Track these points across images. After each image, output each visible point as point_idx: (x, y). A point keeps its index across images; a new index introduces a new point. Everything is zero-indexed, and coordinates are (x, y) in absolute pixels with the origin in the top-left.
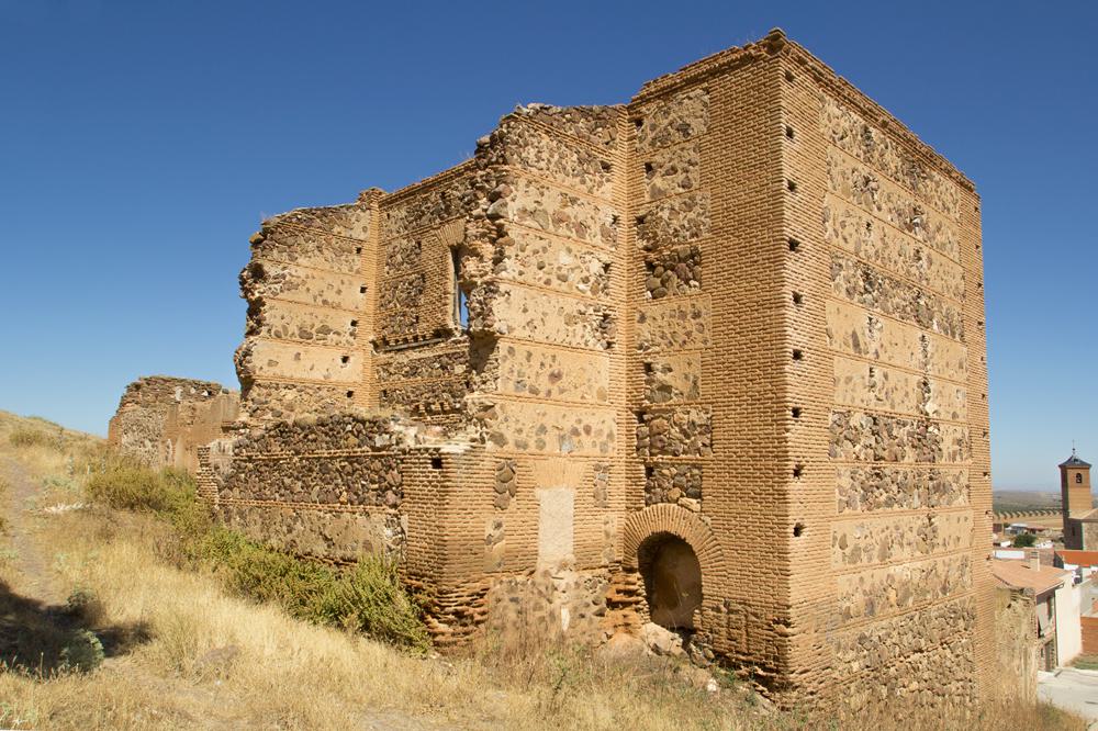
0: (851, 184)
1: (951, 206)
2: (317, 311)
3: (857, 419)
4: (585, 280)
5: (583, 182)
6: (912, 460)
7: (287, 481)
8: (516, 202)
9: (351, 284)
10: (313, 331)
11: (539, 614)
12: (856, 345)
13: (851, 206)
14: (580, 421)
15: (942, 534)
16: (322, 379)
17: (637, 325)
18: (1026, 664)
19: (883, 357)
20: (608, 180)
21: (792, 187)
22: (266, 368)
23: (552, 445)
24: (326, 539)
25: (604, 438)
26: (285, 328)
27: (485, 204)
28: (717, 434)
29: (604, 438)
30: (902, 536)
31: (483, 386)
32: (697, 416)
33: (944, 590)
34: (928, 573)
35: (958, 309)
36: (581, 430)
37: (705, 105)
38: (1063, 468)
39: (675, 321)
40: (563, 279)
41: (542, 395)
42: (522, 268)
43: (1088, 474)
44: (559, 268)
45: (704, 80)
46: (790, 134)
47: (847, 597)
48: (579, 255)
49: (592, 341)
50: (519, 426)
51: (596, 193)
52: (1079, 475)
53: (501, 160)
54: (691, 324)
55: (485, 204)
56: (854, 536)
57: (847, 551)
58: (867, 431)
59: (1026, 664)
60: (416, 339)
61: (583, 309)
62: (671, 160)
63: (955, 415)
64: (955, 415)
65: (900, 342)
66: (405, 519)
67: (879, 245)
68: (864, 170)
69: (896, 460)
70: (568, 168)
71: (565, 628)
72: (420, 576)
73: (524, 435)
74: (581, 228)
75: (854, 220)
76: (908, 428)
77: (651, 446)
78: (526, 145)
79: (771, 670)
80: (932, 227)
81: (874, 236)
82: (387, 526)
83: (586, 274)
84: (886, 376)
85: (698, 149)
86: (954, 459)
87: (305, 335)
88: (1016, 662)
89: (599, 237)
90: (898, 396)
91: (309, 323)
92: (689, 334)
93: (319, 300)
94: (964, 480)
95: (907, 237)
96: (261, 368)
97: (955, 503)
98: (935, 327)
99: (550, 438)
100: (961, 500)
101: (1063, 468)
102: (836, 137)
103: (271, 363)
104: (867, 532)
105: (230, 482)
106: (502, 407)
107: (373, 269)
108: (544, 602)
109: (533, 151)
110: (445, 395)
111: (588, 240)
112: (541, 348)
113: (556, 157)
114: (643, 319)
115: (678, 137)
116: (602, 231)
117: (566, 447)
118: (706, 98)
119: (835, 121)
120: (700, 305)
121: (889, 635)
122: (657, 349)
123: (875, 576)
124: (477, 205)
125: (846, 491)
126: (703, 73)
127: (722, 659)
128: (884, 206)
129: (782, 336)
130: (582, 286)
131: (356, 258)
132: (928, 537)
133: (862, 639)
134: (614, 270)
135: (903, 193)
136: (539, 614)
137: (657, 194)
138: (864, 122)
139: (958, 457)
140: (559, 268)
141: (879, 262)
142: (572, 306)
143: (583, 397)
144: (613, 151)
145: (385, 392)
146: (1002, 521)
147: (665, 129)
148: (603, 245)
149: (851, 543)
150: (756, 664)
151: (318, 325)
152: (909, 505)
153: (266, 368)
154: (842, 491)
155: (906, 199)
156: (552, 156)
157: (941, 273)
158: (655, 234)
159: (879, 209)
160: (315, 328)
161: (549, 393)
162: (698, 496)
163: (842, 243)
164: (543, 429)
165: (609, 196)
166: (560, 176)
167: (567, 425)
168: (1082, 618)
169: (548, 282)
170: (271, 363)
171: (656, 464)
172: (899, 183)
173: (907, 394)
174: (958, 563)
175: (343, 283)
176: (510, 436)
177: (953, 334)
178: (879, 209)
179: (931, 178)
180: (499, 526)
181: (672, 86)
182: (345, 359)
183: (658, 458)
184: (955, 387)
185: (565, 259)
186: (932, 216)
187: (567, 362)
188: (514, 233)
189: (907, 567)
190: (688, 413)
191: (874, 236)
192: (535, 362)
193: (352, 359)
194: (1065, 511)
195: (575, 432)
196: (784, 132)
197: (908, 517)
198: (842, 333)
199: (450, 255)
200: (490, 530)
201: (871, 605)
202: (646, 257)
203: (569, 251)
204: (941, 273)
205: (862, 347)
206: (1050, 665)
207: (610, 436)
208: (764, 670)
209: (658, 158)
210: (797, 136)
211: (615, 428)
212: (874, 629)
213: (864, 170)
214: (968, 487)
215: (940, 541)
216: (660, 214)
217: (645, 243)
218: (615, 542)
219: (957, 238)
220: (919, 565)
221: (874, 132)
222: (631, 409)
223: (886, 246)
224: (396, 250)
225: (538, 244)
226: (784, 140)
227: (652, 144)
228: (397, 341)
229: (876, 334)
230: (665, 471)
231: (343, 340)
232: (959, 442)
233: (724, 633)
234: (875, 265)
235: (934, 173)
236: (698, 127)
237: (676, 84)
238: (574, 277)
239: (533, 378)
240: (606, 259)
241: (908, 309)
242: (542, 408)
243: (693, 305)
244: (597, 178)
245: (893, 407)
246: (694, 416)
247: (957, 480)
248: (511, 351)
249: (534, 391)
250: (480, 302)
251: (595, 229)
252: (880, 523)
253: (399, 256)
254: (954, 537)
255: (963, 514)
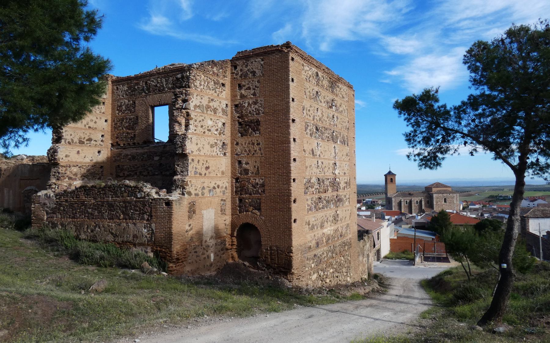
0: (312, 95)
1: (345, 96)
2: (86, 132)
3: (314, 180)
4: (217, 130)
5: (216, 92)
6: (331, 192)
7: (90, 210)
8: (194, 101)
9: (101, 118)
10: (85, 141)
11: (204, 256)
12: (313, 153)
13: (312, 103)
14: (216, 184)
15: (340, 216)
16: (89, 161)
17: (235, 146)
18: (368, 260)
19: (322, 156)
20: (224, 90)
21: (293, 100)
22: (64, 158)
23: (207, 194)
24: (112, 234)
25: (224, 189)
26: (72, 140)
27: (181, 103)
28: (266, 187)
29: (224, 189)
30: (327, 219)
31: (182, 173)
32: (259, 181)
33: (341, 236)
34: (336, 230)
35: (346, 134)
36: (216, 187)
37: (262, 65)
38: (386, 176)
39: (250, 145)
40: (209, 130)
41: (203, 175)
42: (196, 128)
43: (395, 178)
44: (208, 127)
45: (261, 55)
46: (293, 80)
47: (310, 242)
48: (214, 121)
49: (219, 153)
50: (196, 188)
51: (220, 96)
52: (392, 179)
53: (187, 86)
54: (257, 148)
55: (181, 103)
56: (312, 220)
57: (310, 226)
58: (316, 184)
59: (368, 260)
60: (134, 144)
61: (216, 141)
62: (248, 84)
63: (345, 173)
64: (345, 173)
65: (327, 150)
66: (153, 225)
67: (321, 116)
68: (316, 89)
69: (325, 192)
70: (211, 87)
71: (212, 260)
72: (161, 247)
73: (197, 191)
74: (215, 110)
75: (313, 108)
76: (329, 180)
77: (241, 190)
78: (196, 80)
79: (287, 269)
80: (338, 105)
81: (319, 113)
82: (145, 228)
83: (217, 128)
84: (322, 163)
85: (258, 82)
86: (344, 189)
87: (81, 142)
88: (365, 259)
89: (221, 113)
90: (326, 170)
91: (83, 137)
92: (255, 151)
93: (87, 126)
94: (347, 197)
95: (330, 111)
96: (62, 158)
97: (345, 205)
98: (339, 142)
99: (206, 191)
100: (347, 203)
101: (386, 176)
102: (307, 78)
103: (66, 156)
104: (316, 219)
105: (54, 211)
106: (190, 181)
107: (110, 111)
108: (205, 252)
109: (198, 82)
110: (149, 169)
111: (217, 115)
112: (203, 158)
113: (206, 83)
114: (237, 144)
115: (250, 75)
116: (222, 110)
117: (211, 193)
118: (262, 62)
119: (307, 72)
120: (260, 141)
121: (323, 253)
122: (243, 155)
123: (319, 233)
124: (178, 104)
125: (309, 205)
126: (261, 53)
127: (269, 266)
128: (322, 101)
129: (289, 154)
130: (216, 133)
131: (102, 106)
132: (336, 219)
133: (315, 255)
134: (226, 125)
135: (329, 95)
136: (204, 256)
137: (242, 96)
138: (316, 71)
139: (346, 188)
140: (208, 127)
141: (321, 122)
142: (212, 141)
143: (216, 175)
144: (226, 78)
145: (119, 166)
146: (362, 198)
147: (246, 71)
148: (222, 116)
149: (311, 223)
150: (282, 267)
151: (87, 138)
152: (330, 208)
153: (64, 158)
154: (308, 205)
155: (330, 97)
156: (205, 83)
157: (341, 122)
158: (242, 112)
159: (321, 102)
160: (86, 139)
161: (205, 174)
162: (259, 210)
163: (309, 117)
164: (203, 188)
165: (224, 97)
166: (208, 91)
167: (212, 185)
168: (390, 239)
169: (204, 133)
170: (66, 156)
171: (243, 198)
172: (328, 91)
173: (329, 168)
174: (346, 226)
175: (97, 118)
176: (193, 192)
177: (345, 144)
178: (321, 102)
179: (338, 87)
180: (190, 225)
181: (248, 55)
182: (99, 152)
183: (244, 196)
184: (345, 163)
185: (210, 123)
186: (338, 101)
187: (212, 163)
188: (193, 115)
189: (329, 230)
190: (255, 180)
191: (319, 113)
192: (201, 163)
193: (102, 152)
194: (386, 194)
195: (214, 188)
196: (291, 80)
197: (329, 212)
198: (308, 150)
199: (150, 110)
200: (187, 228)
201: (317, 244)
202: (238, 120)
203: (211, 119)
204: (341, 122)
205: (315, 154)
206: (378, 259)
207: (226, 188)
208: (284, 269)
209: (243, 83)
210: (295, 81)
211: (227, 185)
212: (319, 252)
213: (316, 89)
214: (349, 198)
215: (339, 219)
216: (244, 104)
217: (238, 115)
218: (228, 227)
219: (347, 108)
220: (332, 228)
221: (320, 73)
222: (233, 177)
223: (323, 116)
224: (122, 104)
225: (201, 118)
226: (291, 83)
227: (241, 77)
228: (124, 144)
229: (320, 148)
230: (247, 201)
231: (98, 143)
232: (346, 183)
233: (269, 257)
234: (320, 125)
235: (339, 85)
236: (258, 73)
237: (250, 55)
238: (213, 130)
239: (200, 170)
240: (223, 121)
241: (330, 137)
242: (202, 180)
243: (257, 141)
244: (221, 90)
245: (324, 173)
246: (257, 181)
247: (345, 196)
248: (193, 160)
249: (201, 174)
250: (180, 142)
251: (220, 110)
252: (320, 215)
253: (124, 107)
254: (344, 217)
255: (347, 208)
